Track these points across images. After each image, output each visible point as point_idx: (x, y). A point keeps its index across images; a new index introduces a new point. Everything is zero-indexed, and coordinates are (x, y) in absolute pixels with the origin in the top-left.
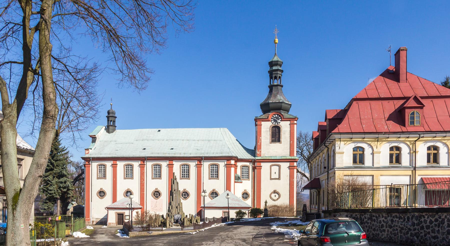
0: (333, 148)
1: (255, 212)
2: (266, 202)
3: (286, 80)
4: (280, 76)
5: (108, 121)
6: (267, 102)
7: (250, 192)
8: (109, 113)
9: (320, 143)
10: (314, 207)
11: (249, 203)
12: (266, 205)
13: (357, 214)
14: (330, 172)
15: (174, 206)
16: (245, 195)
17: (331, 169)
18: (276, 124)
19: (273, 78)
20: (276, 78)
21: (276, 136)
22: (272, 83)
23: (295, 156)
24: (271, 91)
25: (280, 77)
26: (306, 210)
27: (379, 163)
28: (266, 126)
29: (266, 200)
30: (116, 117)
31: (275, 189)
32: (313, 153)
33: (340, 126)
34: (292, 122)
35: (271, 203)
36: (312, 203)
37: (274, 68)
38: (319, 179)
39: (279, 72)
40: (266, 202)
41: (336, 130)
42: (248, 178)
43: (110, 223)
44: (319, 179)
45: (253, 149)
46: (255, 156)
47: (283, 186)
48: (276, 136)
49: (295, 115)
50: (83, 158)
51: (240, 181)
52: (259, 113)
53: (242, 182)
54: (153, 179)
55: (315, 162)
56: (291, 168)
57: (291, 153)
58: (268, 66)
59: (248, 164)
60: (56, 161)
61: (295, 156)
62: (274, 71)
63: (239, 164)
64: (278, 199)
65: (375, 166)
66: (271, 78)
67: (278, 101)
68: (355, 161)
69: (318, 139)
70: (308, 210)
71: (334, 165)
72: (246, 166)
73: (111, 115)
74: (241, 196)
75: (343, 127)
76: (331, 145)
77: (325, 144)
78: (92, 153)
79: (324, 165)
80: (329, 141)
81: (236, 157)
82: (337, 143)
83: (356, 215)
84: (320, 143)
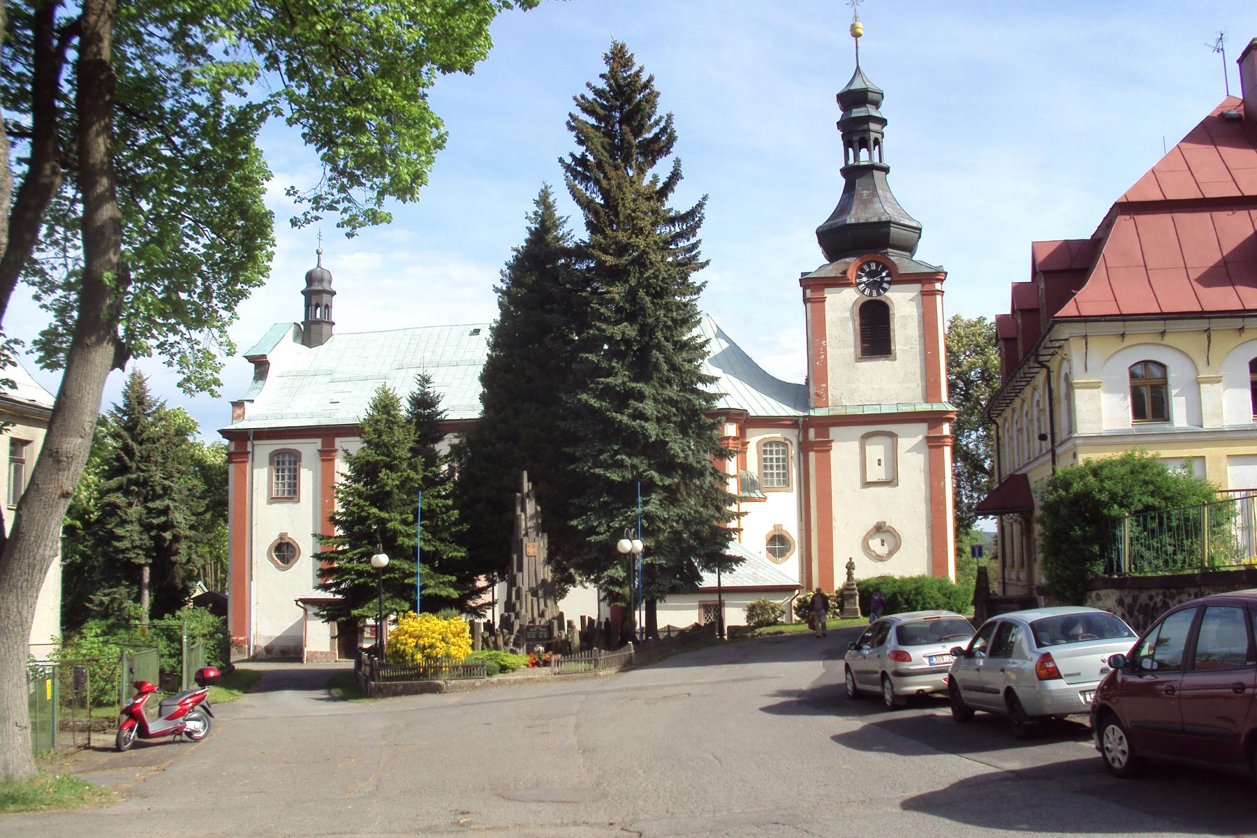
0: (1065, 370)
1: (813, 608)
2: (850, 567)
3: (895, 145)
4: (879, 136)
5: (308, 305)
6: (839, 221)
7: (792, 530)
8: (310, 278)
9: (1021, 356)
10: (1014, 576)
11: (788, 571)
12: (850, 574)
13: (1153, 592)
14: (1058, 451)
15: (525, 588)
16: (778, 544)
17: (1062, 443)
18: (875, 293)
19: (856, 145)
20: (864, 143)
21: (875, 334)
22: (851, 161)
23: (944, 404)
24: (849, 190)
25: (877, 142)
26: (987, 588)
27: (1220, 416)
28: (842, 304)
29: (853, 559)
30: (333, 293)
31: (880, 520)
32: (1002, 389)
33: (1081, 295)
34: (927, 288)
35: (867, 571)
36: (1008, 562)
37: (857, 112)
38: (1025, 476)
39: (873, 126)
40: (850, 567)
41: (1069, 310)
42: (787, 483)
43: (313, 654)
44: (1025, 476)
45: (803, 382)
46: (806, 407)
47: (907, 507)
48: (875, 334)
49: (935, 262)
50: (225, 433)
51: (758, 494)
52: (815, 259)
53: (765, 499)
54: (273, 500)
55: (1010, 420)
56: (934, 443)
57: (930, 392)
58: (837, 106)
59: (777, 434)
60: (141, 443)
61: (944, 404)
62: (858, 117)
63: (755, 438)
64: (891, 553)
65: (1207, 426)
66: (848, 144)
67: (875, 219)
68: (1139, 413)
69: (1015, 339)
70: (995, 587)
71: (1071, 427)
72: (778, 443)
73: (316, 287)
74: (763, 545)
75: (1091, 297)
76: (1058, 358)
77: (1037, 355)
78: (254, 418)
79: (1039, 428)
80: (1049, 345)
81: (742, 413)
82: (1075, 351)
83: (1151, 598)
84: (1021, 356)
